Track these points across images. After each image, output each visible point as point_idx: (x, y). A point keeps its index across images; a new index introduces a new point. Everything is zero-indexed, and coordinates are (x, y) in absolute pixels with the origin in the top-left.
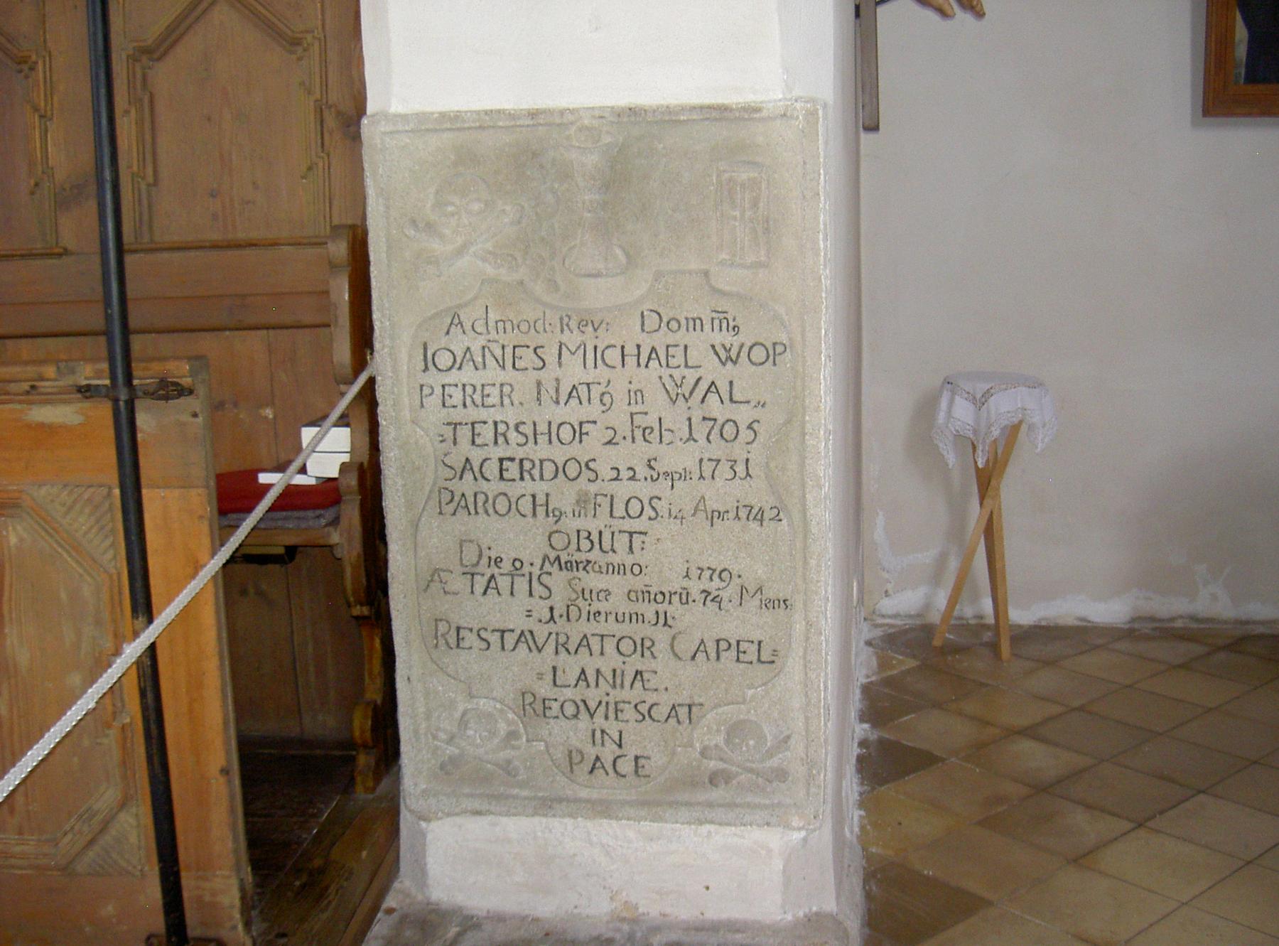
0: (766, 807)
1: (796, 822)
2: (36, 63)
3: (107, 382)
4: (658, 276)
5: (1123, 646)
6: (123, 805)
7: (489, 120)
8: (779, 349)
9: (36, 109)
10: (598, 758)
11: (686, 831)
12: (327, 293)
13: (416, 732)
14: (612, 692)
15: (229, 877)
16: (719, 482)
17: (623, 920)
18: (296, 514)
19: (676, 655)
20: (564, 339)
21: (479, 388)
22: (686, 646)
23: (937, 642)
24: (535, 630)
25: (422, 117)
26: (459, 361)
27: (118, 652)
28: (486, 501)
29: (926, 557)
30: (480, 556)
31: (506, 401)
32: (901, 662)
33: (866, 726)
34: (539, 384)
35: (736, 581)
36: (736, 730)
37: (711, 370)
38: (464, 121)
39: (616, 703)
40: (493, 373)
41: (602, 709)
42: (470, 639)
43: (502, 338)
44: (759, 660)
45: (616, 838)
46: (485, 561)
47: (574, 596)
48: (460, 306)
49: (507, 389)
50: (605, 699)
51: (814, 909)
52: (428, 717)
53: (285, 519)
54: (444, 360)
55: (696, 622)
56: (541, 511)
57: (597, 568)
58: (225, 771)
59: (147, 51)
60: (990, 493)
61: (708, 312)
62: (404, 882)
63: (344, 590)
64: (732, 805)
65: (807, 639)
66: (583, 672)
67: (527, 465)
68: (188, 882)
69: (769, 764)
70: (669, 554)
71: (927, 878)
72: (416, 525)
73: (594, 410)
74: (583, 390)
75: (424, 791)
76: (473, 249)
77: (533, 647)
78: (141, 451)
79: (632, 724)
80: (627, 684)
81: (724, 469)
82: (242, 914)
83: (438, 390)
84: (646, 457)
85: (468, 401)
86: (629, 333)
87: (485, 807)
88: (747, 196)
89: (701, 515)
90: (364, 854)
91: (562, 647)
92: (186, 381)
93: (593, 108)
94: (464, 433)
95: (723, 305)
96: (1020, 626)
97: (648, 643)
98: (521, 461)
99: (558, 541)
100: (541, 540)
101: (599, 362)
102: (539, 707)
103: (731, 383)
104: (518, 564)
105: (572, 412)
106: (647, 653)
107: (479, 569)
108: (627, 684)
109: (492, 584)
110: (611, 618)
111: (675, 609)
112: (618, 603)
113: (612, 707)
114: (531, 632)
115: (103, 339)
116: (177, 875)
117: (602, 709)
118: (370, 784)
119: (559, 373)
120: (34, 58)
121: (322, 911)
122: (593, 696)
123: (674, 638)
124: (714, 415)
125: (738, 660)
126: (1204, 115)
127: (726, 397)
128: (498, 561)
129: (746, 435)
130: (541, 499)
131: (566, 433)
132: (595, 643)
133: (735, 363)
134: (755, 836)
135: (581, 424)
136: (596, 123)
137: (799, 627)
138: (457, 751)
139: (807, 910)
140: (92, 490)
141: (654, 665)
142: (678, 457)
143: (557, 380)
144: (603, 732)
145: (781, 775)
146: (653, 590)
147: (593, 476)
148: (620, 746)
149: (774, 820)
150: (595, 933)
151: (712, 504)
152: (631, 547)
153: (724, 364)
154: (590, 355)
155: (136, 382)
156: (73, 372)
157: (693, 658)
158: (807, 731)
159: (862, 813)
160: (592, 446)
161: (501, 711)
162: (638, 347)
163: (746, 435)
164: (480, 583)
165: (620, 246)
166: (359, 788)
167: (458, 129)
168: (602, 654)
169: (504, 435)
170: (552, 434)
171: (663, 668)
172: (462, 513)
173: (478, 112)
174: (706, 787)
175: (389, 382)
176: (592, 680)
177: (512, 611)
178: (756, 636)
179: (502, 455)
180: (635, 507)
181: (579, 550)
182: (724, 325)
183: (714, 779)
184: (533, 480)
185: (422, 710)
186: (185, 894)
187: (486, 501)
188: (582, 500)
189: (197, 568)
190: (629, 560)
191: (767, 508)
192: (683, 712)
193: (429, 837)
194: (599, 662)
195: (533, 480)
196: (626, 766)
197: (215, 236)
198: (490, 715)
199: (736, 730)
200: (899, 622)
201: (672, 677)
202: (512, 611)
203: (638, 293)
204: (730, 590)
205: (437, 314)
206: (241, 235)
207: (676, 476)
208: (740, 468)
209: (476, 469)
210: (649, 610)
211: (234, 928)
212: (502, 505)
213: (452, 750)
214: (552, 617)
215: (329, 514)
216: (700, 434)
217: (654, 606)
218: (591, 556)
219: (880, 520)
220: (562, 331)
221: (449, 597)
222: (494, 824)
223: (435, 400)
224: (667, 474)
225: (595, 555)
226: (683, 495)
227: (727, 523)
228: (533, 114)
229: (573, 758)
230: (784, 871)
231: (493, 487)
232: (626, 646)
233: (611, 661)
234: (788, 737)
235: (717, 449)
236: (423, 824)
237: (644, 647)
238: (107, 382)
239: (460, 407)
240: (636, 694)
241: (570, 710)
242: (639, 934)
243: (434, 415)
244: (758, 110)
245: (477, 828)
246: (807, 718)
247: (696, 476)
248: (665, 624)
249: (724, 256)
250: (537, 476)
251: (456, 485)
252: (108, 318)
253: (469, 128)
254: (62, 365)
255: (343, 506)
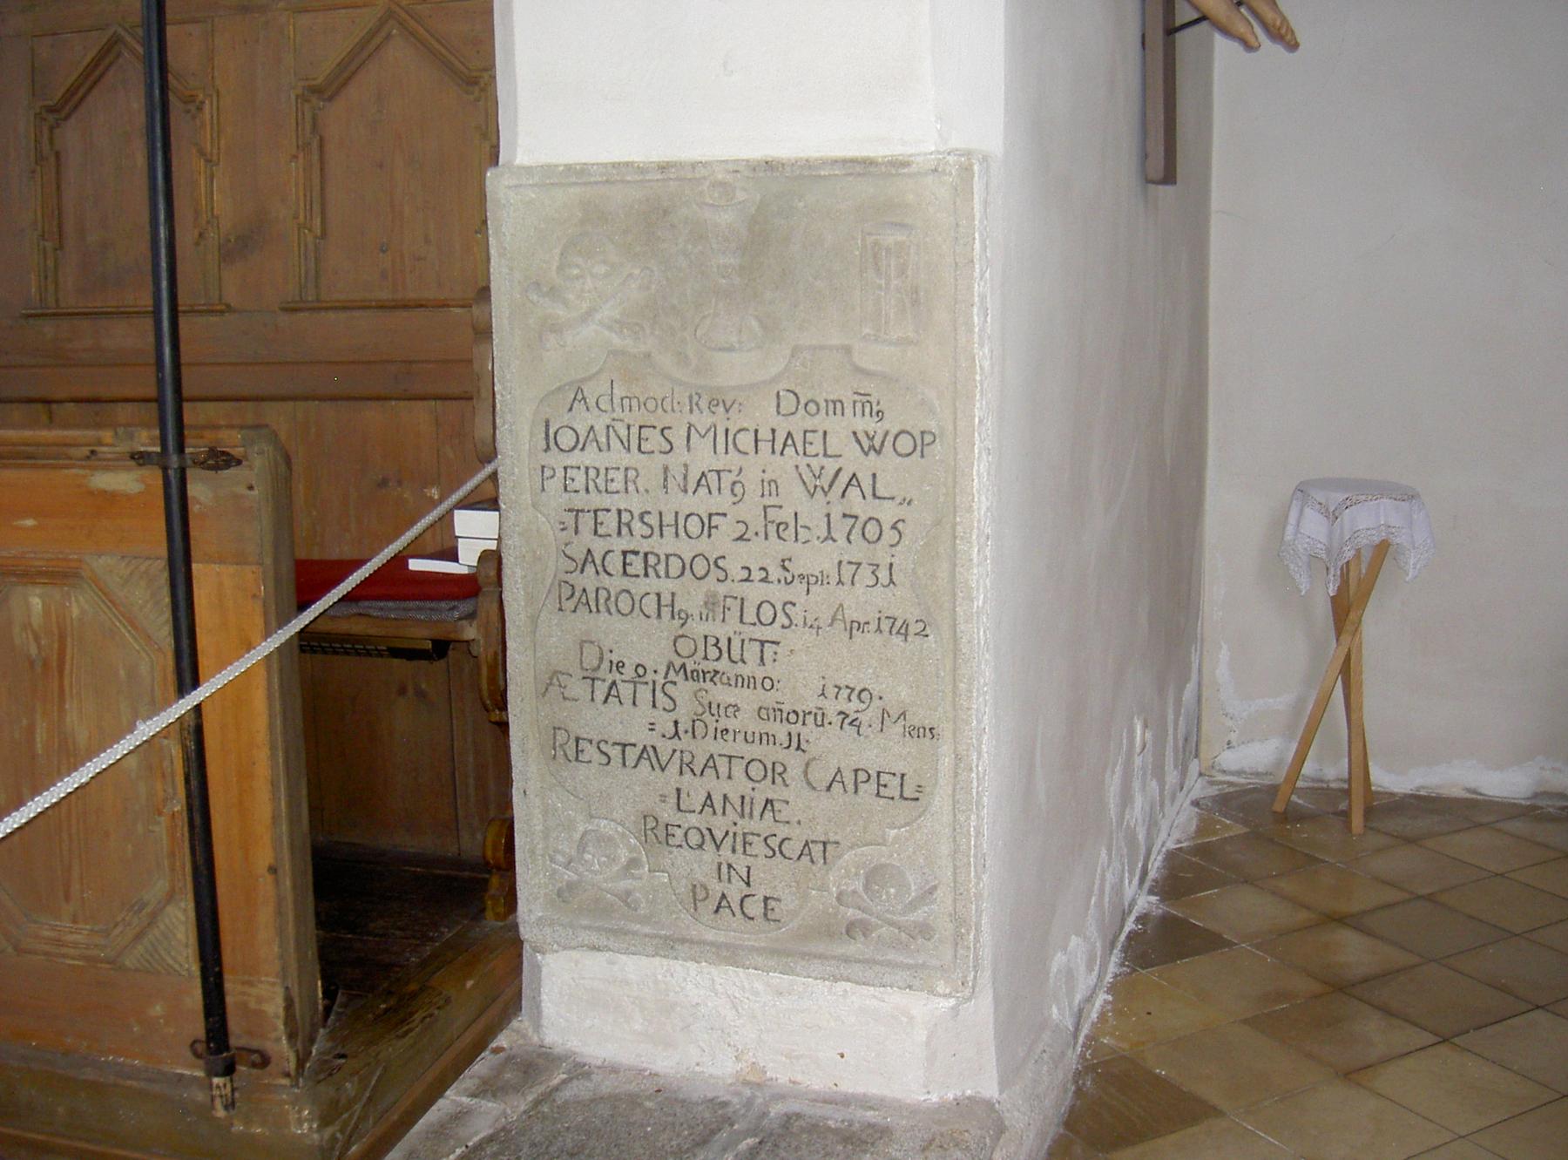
0: (909, 967)
1: (941, 987)
2: (203, 103)
3: (158, 449)
4: (795, 351)
5: (1517, 826)
6: (170, 897)
7: (618, 172)
8: (928, 439)
9: (202, 153)
10: (724, 896)
11: (821, 987)
12: (470, 361)
13: (532, 852)
14: (740, 822)
15: (273, 984)
16: (859, 588)
17: (746, 1083)
18: (428, 604)
19: (809, 783)
20: (694, 419)
21: (603, 471)
22: (821, 776)
23: (1279, 807)
24: (659, 746)
25: (548, 170)
26: (582, 440)
27: (131, 729)
28: (608, 599)
29: (1281, 702)
30: (601, 659)
31: (631, 487)
32: (1227, 827)
33: (1154, 899)
34: (666, 469)
35: (876, 702)
36: (875, 876)
37: (853, 460)
38: (590, 175)
39: (744, 834)
40: (618, 456)
41: (730, 839)
42: (590, 752)
43: (626, 416)
44: (902, 796)
45: (743, 989)
46: (606, 665)
47: (700, 710)
48: (584, 380)
49: (632, 474)
50: (732, 830)
51: (969, 1092)
52: (546, 837)
53: (419, 609)
54: (566, 439)
55: (833, 748)
56: (666, 611)
57: (725, 679)
58: (273, 870)
59: (317, 91)
60: (1349, 627)
61: (850, 393)
62: (521, 1023)
63: (480, 690)
64: (870, 962)
65: (956, 775)
66: (709, 796)
67: (652, 560)
68: (230, 985)
69: (912, 917)
70: (806, 667)
71: (1158, 1077)
72: (534, 620)
73: (722, 502)
74: (712, 477)
75: (540, 918)
76: (598, 317)
77: (656, 766)
78: (192, 523)
79: (761, 861)
80: (757, 813)
81: (865, 573)
82: (286, 1024)
83: (560, 473)
84: (780, 557)
85: (591, 485)
86: (762, 415)
87: (603, 941)
88: (893, 263)
89: (839, 625)
90: (469, 984)
91: (686, 767)
92: (237, 452)
93: (726, 162)
94: (587, 521)
95: (867, 386)
96: (1392, 794)
97: (779, 769)
98: (646, 555)
99: (685, 647)
100: (666, 644)
101: (731, 446)
102: (661, 833)
103: (874, 475)
104: (641, 671)
105: (701, 503)
106: (778, 780)
107: (600, 674)
108: (757, 813)
109: (614, 692)
110: (740, 737)
111: (809, 731)
112: (746, 721)
113: (739, 839)
114: (654, 748)
115: (154, 405)
116: (220, 976)
117: (730, 839)
118: (501, 910)
119: (686, 457)
120: (201, 97)
121: (399, 1037)
122: (720, 824)
123: (807, 765)
124: (856, 511)
125: (878, 794)
126: (1175, 183)
127: (868, 491)
128: (620, 665)
129: (889, 536)
130: (666, 599)
131: (694, 526)
132: (722, 765)
133: (878, 452)
134: (895, 998)
135: (710, 515)
136: (729, 178)
137: (946, 762)
138: (575, 877)
139: (959, 1094)
140: (148, 563)
141: (786, 794)
142: (816, 558)
143: (686, 466)
144: (730, 866)
145: (925, 930)
146: (786, 708)
147: (722, 575)
148: (748, 884)
149: (917, 983)
150: (710, 1095)
151: (852, 614)
152: (762, 659)
153: (866, 454)
154: (721, 439)
155: (188, 450)
156: (131, 437)
157: (829, 788)
158: (955, 882)
159: (1110, 998)
160: (721, 544)
161: (623, 835)
162: (773, 431)
163: (889, 536)
164: (601, 689)
165: (757, 318)
166: (489, 914)
167: (585, 184)
168: (730, 777)
169: (628, 525)
170: (679, 526)
171: (796, 798)
172: (582, 609)
173: (605, 165)
174: (850, 938)
175: (508, 461)
176: (718, 806)
177: (633, 722)
178: (899, 767)
179: (626, 548)
180: (767, 614)
181: (706, 658)
182: (867, 410)
183: (851, 929)
184: (658, 576)
185: (539, 828)
186: (229, 1000)
187: (608, 599)
188: (710, 602)
189: (249, 647)
190: (760, 673)
191: (912, 620)
192: (817, 849)
193: (545, 971)
194: (724, 787)
195: (658, 576)
196: (754, 907)
197: (385, 295)
198: (610, 839)
199: (875, 876)
200: (1242, 781)
201: (806, 811)
202: (633, 722)
203: (774, 371)
204: (869, 713)
205: (559, 389)
206: (412, 295)
207: (813, 580)
208: (883, 574)
209: (598, 562)
210: (780, 731)
211: (278, 1040)
212: (625, 604)
213: (570, 875)
214: (677, 733)
215: (465, 607)
216: (840, 536)
217: (786, 727)
218: (719, 666)
219: (1224, 655)
220: (691, 411)
221: (568, 703)
222: (611, 963)
223: (554, 485)
224: (801, 576)
225: (723, 665)
226: (819, 602)
227: (869, 636)
228: (663, 167)
229: (697, 894)
230: (928, 1044)
231: (616, 583)
232: (756, 771)
233: (739, 786)
234: (935, 888)
235: (858, 551)
236: (539, 957)
237: (775, 773)
238: (158, 449)
239: (583, 492)
240: (765, 825)
241: (694, 838)
242: (760, 1100)
243: (555, 498)
244: (906, 164)
245: (594, 964)
246: (955, 867)
247: (834, 579)
248: (798, 748)
249: (867, 330)
250: (662, 573)
251: (579, 580)
252: (160, 382)
253: (596, 183)
254: (121, 431)
255: (481, 598)
